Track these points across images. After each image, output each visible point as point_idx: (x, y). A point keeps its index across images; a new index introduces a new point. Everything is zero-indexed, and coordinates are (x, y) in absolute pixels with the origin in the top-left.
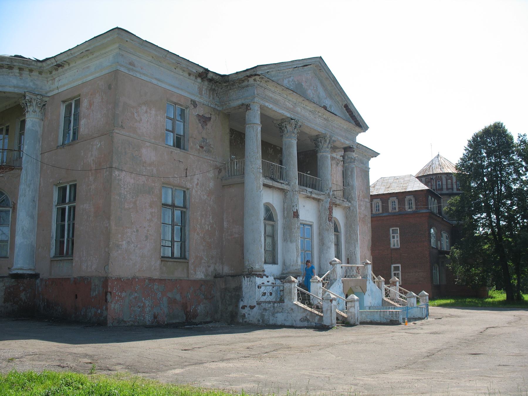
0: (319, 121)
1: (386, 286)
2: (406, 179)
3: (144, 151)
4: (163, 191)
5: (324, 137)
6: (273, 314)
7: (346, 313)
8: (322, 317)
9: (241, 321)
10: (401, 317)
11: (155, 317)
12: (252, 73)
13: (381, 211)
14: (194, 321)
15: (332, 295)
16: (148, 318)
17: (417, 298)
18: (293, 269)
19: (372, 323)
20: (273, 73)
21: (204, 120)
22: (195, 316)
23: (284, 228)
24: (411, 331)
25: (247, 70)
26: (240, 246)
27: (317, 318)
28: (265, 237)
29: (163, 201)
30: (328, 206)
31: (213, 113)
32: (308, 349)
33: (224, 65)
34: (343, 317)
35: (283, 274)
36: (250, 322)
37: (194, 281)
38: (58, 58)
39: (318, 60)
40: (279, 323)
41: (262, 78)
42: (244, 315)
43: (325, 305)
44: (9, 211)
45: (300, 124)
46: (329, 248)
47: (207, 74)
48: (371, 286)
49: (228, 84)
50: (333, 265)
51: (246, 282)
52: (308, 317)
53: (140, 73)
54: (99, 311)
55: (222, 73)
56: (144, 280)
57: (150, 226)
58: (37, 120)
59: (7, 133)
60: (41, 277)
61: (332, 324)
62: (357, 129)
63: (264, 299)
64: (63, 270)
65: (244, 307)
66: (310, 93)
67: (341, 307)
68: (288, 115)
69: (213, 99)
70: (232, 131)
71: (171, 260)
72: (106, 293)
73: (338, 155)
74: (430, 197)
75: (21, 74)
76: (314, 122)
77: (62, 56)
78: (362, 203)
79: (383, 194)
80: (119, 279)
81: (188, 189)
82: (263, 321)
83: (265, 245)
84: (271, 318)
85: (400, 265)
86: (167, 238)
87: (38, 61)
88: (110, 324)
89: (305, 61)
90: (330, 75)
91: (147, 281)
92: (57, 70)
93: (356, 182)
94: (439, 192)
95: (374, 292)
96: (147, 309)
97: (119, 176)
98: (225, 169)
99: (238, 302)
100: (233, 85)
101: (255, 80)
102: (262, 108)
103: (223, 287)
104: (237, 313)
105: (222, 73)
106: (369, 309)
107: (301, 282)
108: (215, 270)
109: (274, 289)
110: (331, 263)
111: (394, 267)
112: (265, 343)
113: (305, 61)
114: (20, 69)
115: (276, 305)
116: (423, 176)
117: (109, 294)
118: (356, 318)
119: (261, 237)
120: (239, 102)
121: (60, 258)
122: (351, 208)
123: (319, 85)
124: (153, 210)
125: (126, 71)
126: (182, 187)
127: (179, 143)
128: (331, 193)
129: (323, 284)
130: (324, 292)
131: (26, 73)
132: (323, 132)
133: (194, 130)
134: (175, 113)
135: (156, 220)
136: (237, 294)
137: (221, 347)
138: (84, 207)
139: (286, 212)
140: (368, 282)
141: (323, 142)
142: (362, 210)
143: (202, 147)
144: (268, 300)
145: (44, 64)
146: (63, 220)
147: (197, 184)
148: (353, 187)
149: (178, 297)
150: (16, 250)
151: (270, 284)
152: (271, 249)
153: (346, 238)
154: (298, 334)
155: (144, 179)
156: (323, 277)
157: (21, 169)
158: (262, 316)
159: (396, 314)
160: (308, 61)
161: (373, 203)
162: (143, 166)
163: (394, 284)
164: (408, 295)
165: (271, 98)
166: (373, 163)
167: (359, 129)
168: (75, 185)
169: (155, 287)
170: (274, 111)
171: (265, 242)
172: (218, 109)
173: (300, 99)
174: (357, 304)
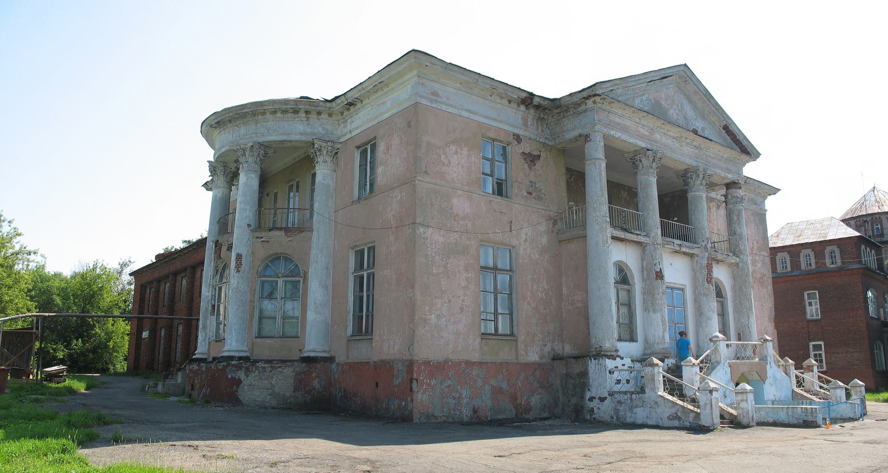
0: (688, 150)
1: (797, 372)
2: (825, 223)
3: (455, 201)
4: (482, 251)
5: (696, 171)
6: (631, 409)
7: (735, 408)
8: (698, 414)
9: (588, 417)
10: (820, 416)
11: (475, 411)
12: (591, 94)
13: (789, 269)
14: (527, 416)
15: (717, 387)
16: (466, 413)
17: (846, 389)
18: (658, 347)
19: (775, 424)
20: (619, 91)
21: (532, 159)
22: (528, 410)
23: (644, 294)
24: (834, 438)
25: (583, 90)
26: (584, 315)
27: (692, 415)
28: (618, 307)
29: (482, 263)
30: (705, 262)
31: (543, 150)
32: (670, 459)
33: (553, 86)
34: (731, 414)
35: (644, 354)
36: (600, 419)
37: (526, 364)
38: (349, 95)
39: (682, 68)
40: (640, 422)
41: (605, 99)
42: (592, 410)
43: (701, 397)
44: (299, 281)
45: (659, 155)
46: (710, 319)
47: (532, 99)
48: (774, 371)
49: (560, 110)
50: (715, 342)
51: (593, 366)
52: (679, 414)
53: (447, 105)
54: (403, 403)
55: (552, 97)
56: (460, 363)
57: (465, 295)
58: (329, 172)
59: (297, 191)
60: (337, 361)
61: (713, 425)
62: (744, 157)
63: (617, 388)
64: (362, 352)
65: (591, 399)
66: (673, 113)
67: (728, 401)
68: (643, 145)
69: (543, 131)
70: (570, 171)
71: (494, 337)
72: (411, 381)
73: (718, 194)
74: (863, 247)
75: (308, 119)
76: (681, 152)
77: (352, 93)
78: (757, 258)
79: (792, 246)
80: (427, 363)
81: (514, 247)
82: (618, 418)
83: (618, 317)
84: (629, 414)
85: (822, 343)
86: (488, 289)
87: (327, 101)
88: (416, 420)
89: (663, 72)
90: (700, 86)
91: (463, 364)
92: (348, 109)
93: (747, 230)
94: (879, 239)
95: (779, 381)
96: (464, 401)
97: (424, 233)
98: (561, 219)
99: (583, 391)
100: (566, 111)
101: (594, 102)
102: (606, 137)
103: (564, 372)
104: (582, 407)
105: (551, 96)
106: (773, 404)
107: (670, 365)
108: (553, 349)
109: (632, 375)
110: (711, 340)
111: (814, 345)
112: (610, 449)
113: (663, 72)
114: (307, 112)
115: (634, 396)
116: (852, 218)
117: (415, 381)
118: (750, 416)
119: (611, 305)
120: (576, 133)
121: (358, 338)
122: (740, 265)
123: (685, 102)
124: (470, 275)
125: (429, 104)
126: (506, 245)
127: (500, 189)
128: (709, 245)
129: (701, 368)
130: (703, 380)
131: (313, 116)
132: (694, 164)
133: (519, 172)
134: (493, 152)
135: (473, 287)
136: (582, 381)
137: (549, 453)
138: (384, 274)
139: (645, 272)
140: (768, 366)
141: (694, 177)
142: (757, 266)
143: (530, 194)
144: (624, 389)
145: (334, 104)
146: (361, 290)
147: (526, 240)
148: (741, 236)
149: (505, 386)
150: (308, 328)
151: (626, 367)
152: (627, 322)
153: (644, 301)
154: (662, 438)
155: (456, 236)
156: (701, 358)
157: (311, 230)
158: (617, 411)
159: (812, 412)
160: (669, 71)
161: (778, 258)
162: (455, 220)
163: (810, 369)
164: (831, 385)
165: (618, 124)
166: (770, 202)
167: (747, 158)
168: (374, 247)
169: (474, 373)
170: (623, 141)
171: (618, 313)
172: (550, 143)
173: (659, 123)
174: (751, 397)
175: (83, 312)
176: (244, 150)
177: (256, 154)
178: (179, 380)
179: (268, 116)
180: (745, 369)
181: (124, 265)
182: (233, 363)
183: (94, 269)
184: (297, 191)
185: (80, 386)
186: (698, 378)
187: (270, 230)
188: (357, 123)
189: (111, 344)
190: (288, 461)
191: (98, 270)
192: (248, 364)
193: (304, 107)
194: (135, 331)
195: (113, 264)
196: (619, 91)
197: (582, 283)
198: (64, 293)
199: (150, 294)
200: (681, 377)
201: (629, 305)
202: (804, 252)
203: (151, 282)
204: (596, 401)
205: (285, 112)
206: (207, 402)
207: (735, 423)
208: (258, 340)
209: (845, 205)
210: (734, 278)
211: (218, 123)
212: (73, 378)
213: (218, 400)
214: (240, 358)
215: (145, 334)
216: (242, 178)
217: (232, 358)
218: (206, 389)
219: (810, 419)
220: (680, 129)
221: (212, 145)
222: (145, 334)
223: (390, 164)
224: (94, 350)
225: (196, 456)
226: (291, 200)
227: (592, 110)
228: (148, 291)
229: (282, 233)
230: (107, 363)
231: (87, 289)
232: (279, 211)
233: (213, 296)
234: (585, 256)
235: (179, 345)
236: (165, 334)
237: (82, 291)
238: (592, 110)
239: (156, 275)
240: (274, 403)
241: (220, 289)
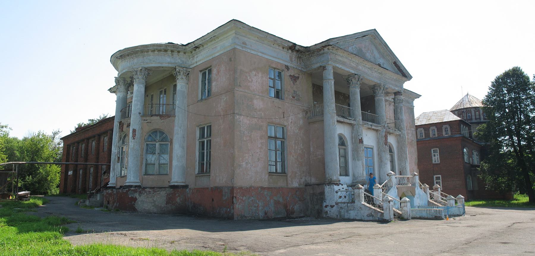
0: (375, 74)
1: (430, 191)
2: (443, 113)
3: (255, 101)
4: (269, 128)
5: (379, 86)
6: (347, 211)
8: (383, 213)
9: (325, 216)
10: (443, 214)
11: (266, 214)
13: (424, 137)
15: (390, 198)
16: (261, 214)
18: (360, 179)
19: (421, 218)
20: (341, 43)
21: (294, 78)
22: (293, 213)
24: (452, 225)
25: (323, 42)
26: (322, 163)
27: (379, 214)
29: (269, 135)
30: (384, 134)
35: (353, 183)
38: (196, 42)
40: (352, 218)
42: (327, 212)
43: (385, 205)
45: (361, 77)
48: (418, 191)
50: (390, 176)
53: (250, 49)
55: (305, 46)
56: (258, 188)
57: (261, 152)
60: (189, 187)
61: (390, 219)
62: (404, 78)
63: (340, 200)
64: (204, 182)
65: (326, 206)
66: (368, 55)
67: (396, 206)
68: (353, 72)
70: (314, 85)
73: (390, 98)
74: (462, 125)
75: (172, 55)
76: (372, 75)
80: (241, 188)
84: (346, 214)
85: (440, 176)
87: (183, 45)
88: (235, 219)
92: (195, 50)
93: (404, 117)
95: (421, 196)
98: (310, 111)
99: (322, 202)
100: (313, 53)
101: (328, 49)
102: (334, 68)
103: (312, 192)
104: (321, 211)
108: (306, 181)
110: (387, 175)
114: (172, 51)
115: (349, 204)
119: (336, 157)
120: (318, 65)
125: (241, 49)
126: (282, 125)
127: (278, 95)
128: (386, 125)
129: (383, 190)
130: (384, 196)
131: (175, 54)
132: (379, 82)
133: (288, 85)
137: (311, 234)
138: (217, 141)
140: (416, 188)
142: (410, 136)
143: (294, 97)
144: (343, 201)
145: (187, 47)
146: (203, 149)
147: (291, 122)
149: (281, 200)
150: (173, 170)
153: (353, 155)
155: (256, 120)
157: (174, 116)
158: (340, 212)
161: (418, 131)
163: (436, 189)
165: (340, 61)
166: (416, 102)
167: (406, 79)
168: (210, 126)
169: (265, 193)
172: (304, 70)
174: (409, 204)
175: (32, 160)
176: (136, 72)
177: (143, 74)
178: (98, 199)
179: (150, 53)
180: (404, 190)
181: (55, 134)
182: (132, 189)
183: (38, 136)
184: (165, 94)
185: (40, 203)
186: (381, 195)
187: (151, 116)
188: (200, 58)
189: (49, 178)
190: (179, 241)
191: (41, 137)
192: (141, 189)
193: (170, 48)
194: (64, 171)
195: (49, 133)
196: (341, 43)
197: (321, 144)
198: (21, 150)
199: (73, 150)
200: (372, 194)
201: (345, 156)
202: (432, 128)
203: (74, 143)
204: (329, 208)
205: (160, 51)
206: (117, 210)
207: (401, 218)
208: (145, 176)
209: (451, 104)
210: (398, 142)
211: (121, 56)
212: (35, 198)
213: (124, 209)
214: (136, 186)
215: (70, 173)
216: (136, 87)
217: (131, 186)
218: (117, 204)
219: (438, 215)
220: (372, 64)
221: (117, 68)
222: (70, 173)
223: (219, 81)
224: (39, 182)
225: (127, 239)
226: (161, 99)
227: (327, 53)
228: (71, 148)
229: (159, 117)
230: (46, 189)
231: (34, 148)
232: (154, 106)
233: (119, 152)
234: (323, 131)
235: (91, 179)
236: (83, 173)
237: (32, 148)
238: (327, 53)
239: (77, 139)
240: (155, 210)
241: (122, 148)
